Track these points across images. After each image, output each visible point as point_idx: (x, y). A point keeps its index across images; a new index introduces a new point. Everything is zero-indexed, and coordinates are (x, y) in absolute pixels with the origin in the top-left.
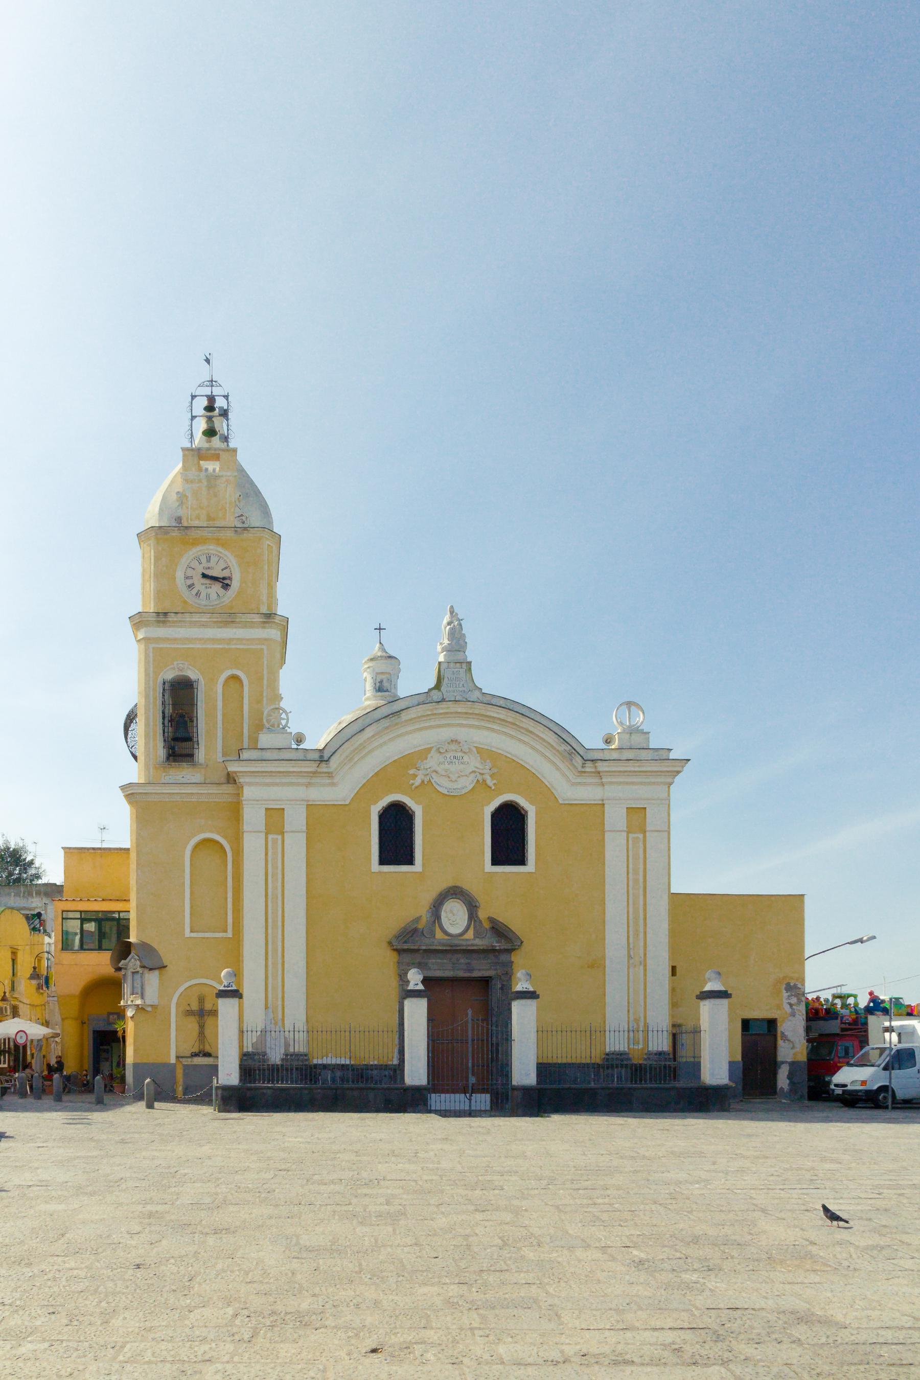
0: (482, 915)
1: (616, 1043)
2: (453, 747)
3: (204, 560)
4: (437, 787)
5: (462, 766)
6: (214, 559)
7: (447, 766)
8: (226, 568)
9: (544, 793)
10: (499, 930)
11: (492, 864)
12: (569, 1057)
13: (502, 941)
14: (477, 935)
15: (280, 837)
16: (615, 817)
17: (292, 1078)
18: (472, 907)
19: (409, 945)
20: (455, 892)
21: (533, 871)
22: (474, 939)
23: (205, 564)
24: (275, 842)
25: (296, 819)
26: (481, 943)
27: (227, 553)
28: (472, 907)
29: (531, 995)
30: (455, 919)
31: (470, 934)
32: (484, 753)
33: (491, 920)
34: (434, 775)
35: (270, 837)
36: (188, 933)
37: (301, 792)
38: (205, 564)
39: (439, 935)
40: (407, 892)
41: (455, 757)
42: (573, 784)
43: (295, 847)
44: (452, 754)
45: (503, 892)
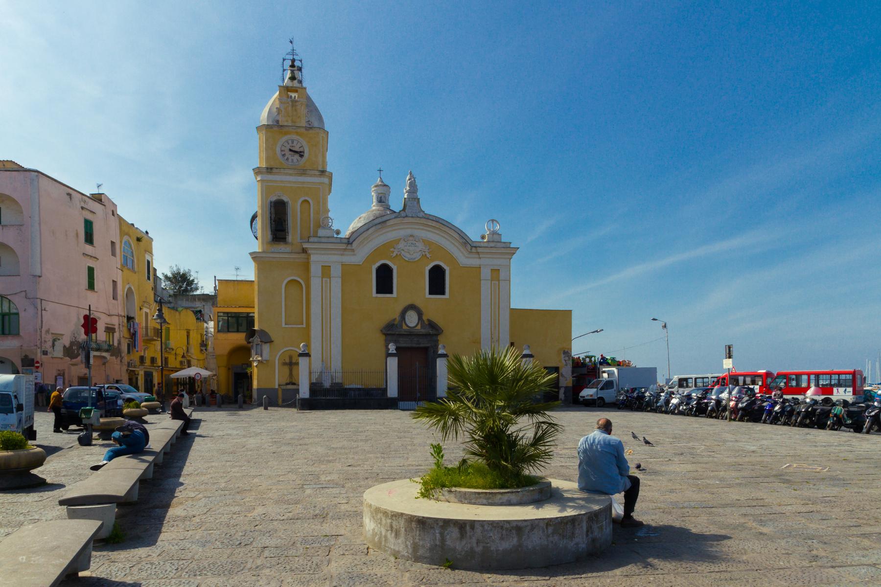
0: (425, 318)
3: (290, 142)
9: (453, 261)
10: (432, 325)
16: (486, 273)
18: (420, 314)
19: (391, 331)
20: (412, 307)
25: (336, 271)
26: (423, 331)
28: (420, 314)
30: (412, 320)
31: (419, 327)
32: (427, 243)
33: (429, 320)
39: (404, 327)
40: (390, 307)
43: (336, 284)
45: (434, 307)
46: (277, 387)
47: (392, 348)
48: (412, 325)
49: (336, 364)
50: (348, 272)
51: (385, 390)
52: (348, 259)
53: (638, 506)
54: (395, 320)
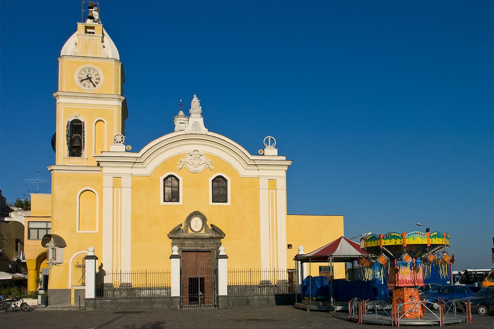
0: (208, 223)
1: (265, 277)
2: (196, 153)
3: (87, 70)
4: (189, 169)
5: (199, 161)
6: (92, 71)
7: (193, 161)
8: (97, 75)
9: (234, 172)
10: (214, 229)
11: (179, 202)
12: (160, 284)
13: (217, 234)
14: (206, 232)
15: (274, 191)
16: (264, 183)
17: (240, 287)
18: (204, 219)
19: (176, 235)
20: (196, 214)
21: (230, 205)
22: (205, 233)
23: (88, 73)
24: (117, 191)
25: (127, 182)
26: (207, 235)
27: (97, 68)
28: (204, 219)
29: (225, 257)
30: (196, 224)
31: (203, 231)
32: (208, 155)
33: (212, 225)
34: (187, 164)
35: (115, 190)
36: (77, 231)
37: (128, 171)
38: (88, 73)
39: (190, 231)
40: (177, 214)
41: (196, 157)
42: (246, 169)
43: (126, 194)
44: (195, 156)
45: (217, 214)
46: (70, 288)
47: (176, 250)
48: (196, 230)
49: (126, 267)
50: (138, 184)
51: (168, 289)
52: (138, 171)
53: (45, 227)
54: (181, 225)
